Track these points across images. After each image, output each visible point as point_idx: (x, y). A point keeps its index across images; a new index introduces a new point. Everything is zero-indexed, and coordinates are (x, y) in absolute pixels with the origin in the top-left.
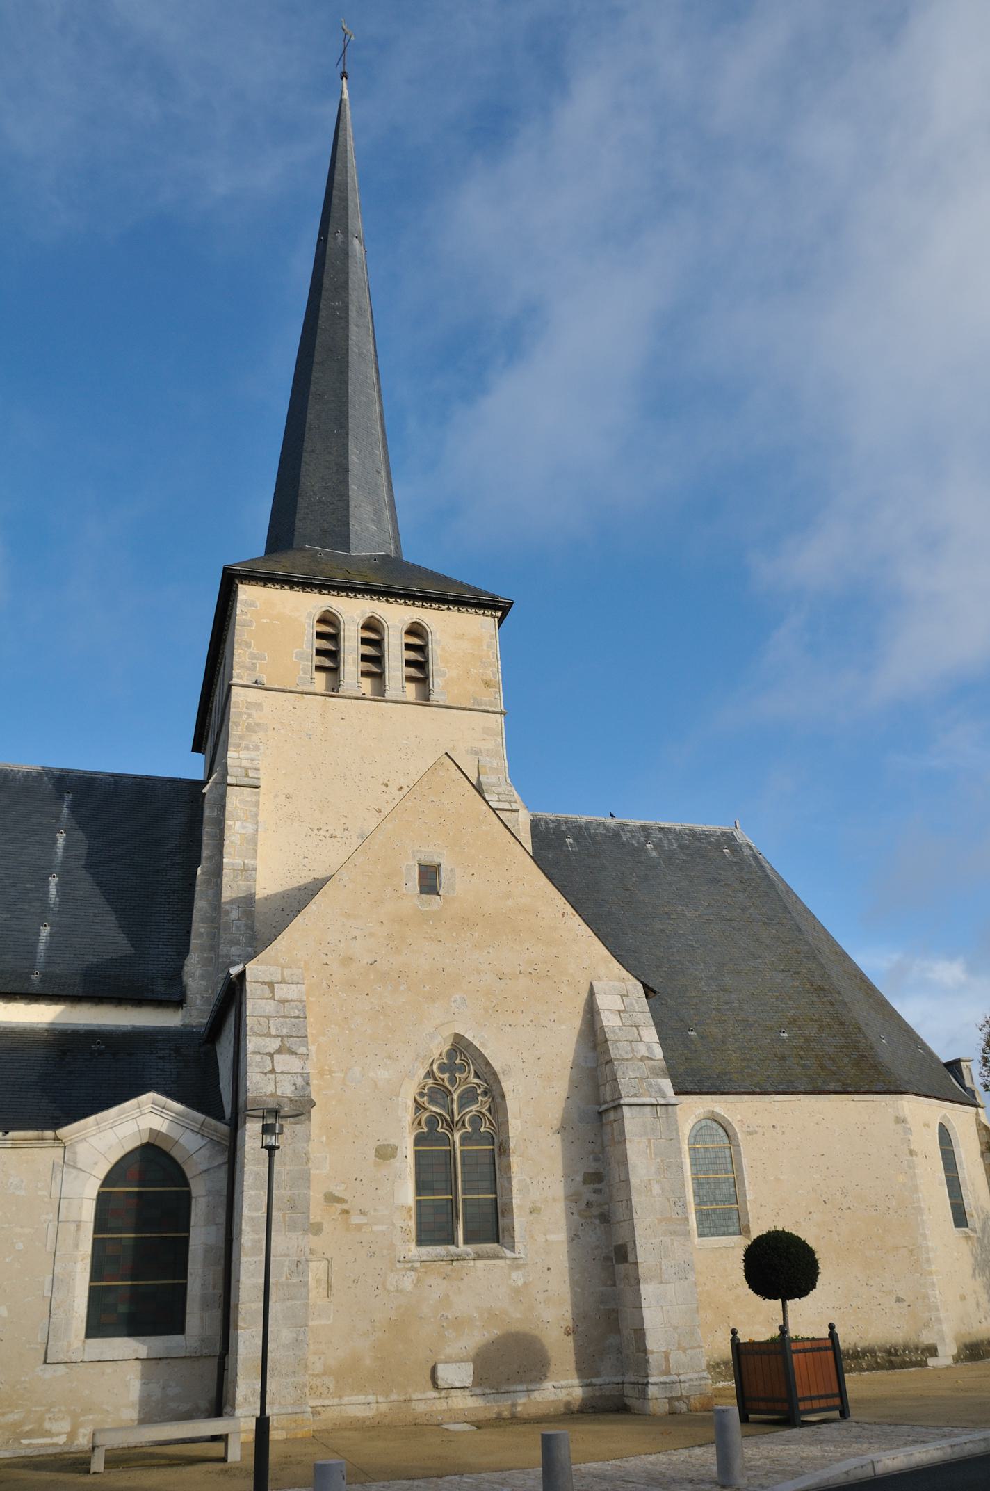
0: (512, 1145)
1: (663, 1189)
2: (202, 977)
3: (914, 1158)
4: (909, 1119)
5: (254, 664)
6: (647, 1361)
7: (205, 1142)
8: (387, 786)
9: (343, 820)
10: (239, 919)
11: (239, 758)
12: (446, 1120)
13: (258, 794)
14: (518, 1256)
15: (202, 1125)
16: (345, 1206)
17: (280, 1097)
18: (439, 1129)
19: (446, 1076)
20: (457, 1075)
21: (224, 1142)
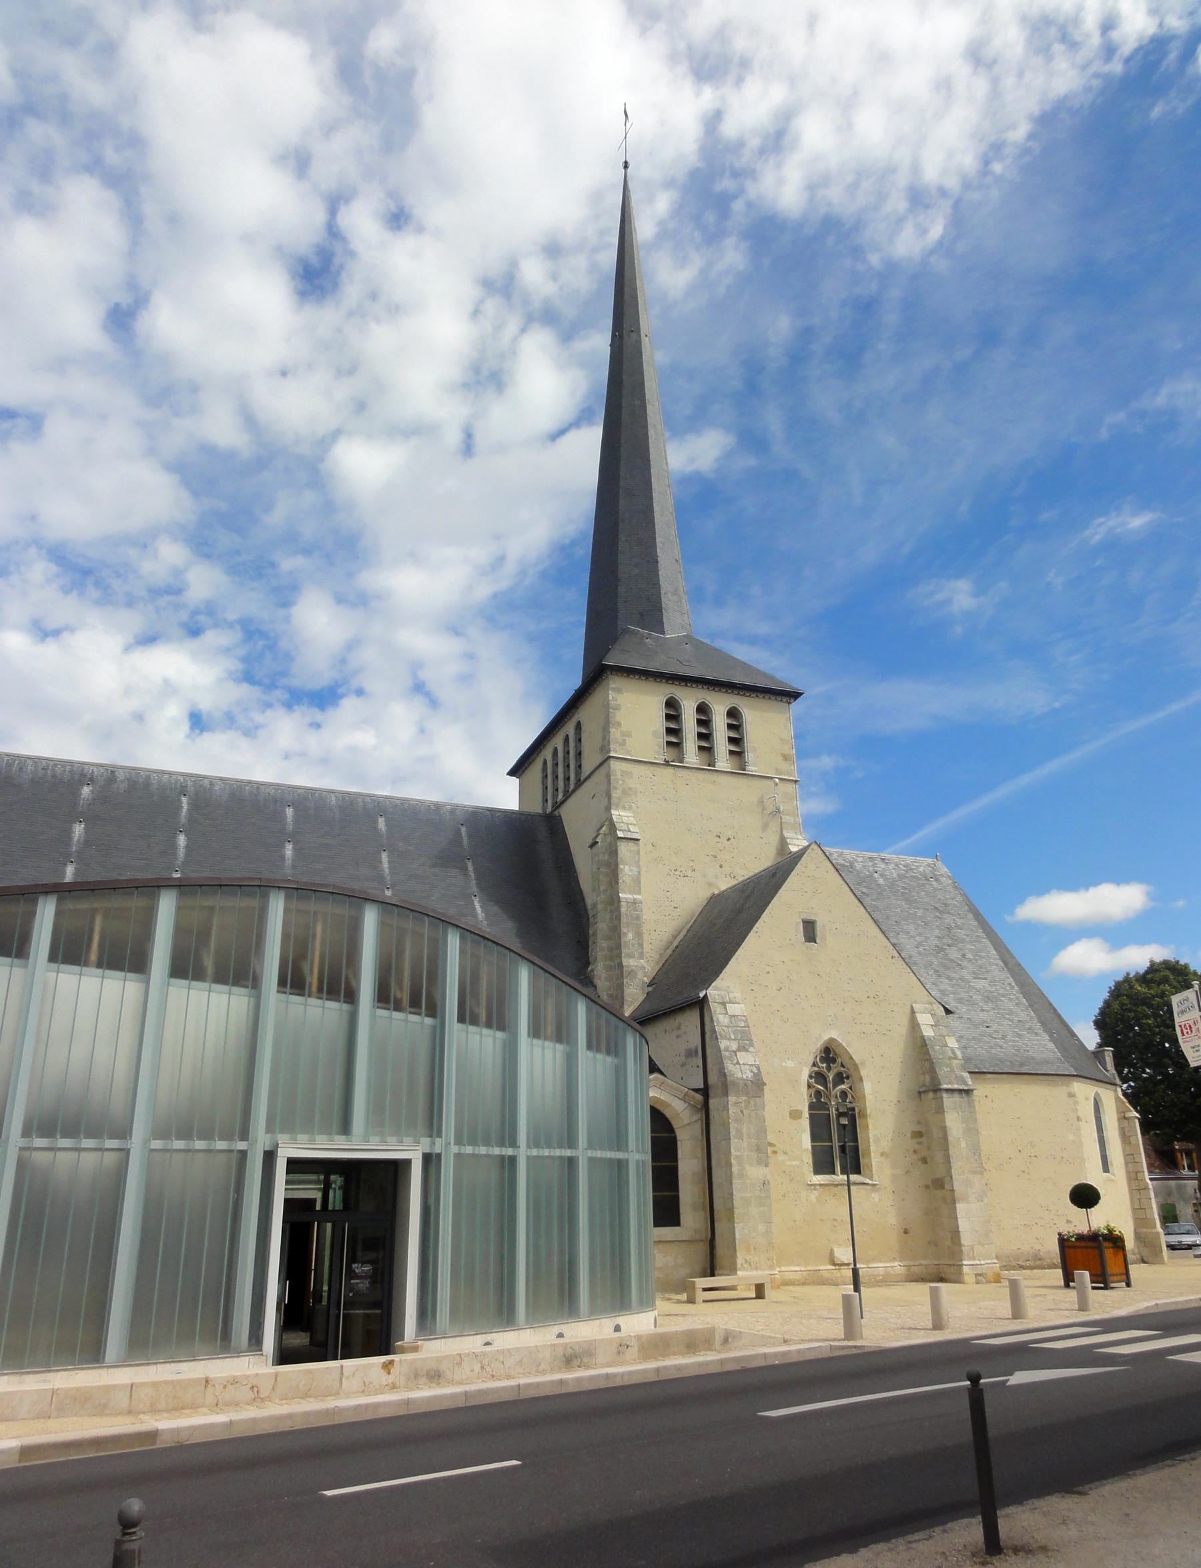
0: (868, 1112)
1: (967, 1144)
2: (607, 979)
3: (1080, 1122)
4: (1077, 1095)
5: (624, 740)
6: (962, 1251)
7: (686, 1105)
8: (719, 837)
9: (691, 864)
10: (633, 939)
11: (620, 815)
12: (827, 1095)
13: (638, 845)
14: (876, 1183)
15: (685, 1095)
16: (775, 1149)
17: (745, 1080)
18: (822, 1100)
19: (824, 1065)
20: (831, 1065)
21: (698, 1106)
